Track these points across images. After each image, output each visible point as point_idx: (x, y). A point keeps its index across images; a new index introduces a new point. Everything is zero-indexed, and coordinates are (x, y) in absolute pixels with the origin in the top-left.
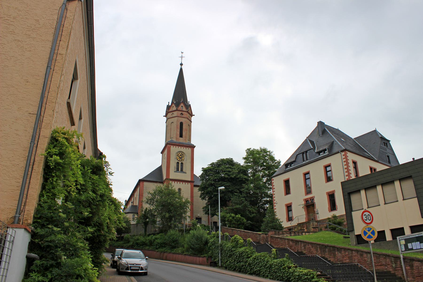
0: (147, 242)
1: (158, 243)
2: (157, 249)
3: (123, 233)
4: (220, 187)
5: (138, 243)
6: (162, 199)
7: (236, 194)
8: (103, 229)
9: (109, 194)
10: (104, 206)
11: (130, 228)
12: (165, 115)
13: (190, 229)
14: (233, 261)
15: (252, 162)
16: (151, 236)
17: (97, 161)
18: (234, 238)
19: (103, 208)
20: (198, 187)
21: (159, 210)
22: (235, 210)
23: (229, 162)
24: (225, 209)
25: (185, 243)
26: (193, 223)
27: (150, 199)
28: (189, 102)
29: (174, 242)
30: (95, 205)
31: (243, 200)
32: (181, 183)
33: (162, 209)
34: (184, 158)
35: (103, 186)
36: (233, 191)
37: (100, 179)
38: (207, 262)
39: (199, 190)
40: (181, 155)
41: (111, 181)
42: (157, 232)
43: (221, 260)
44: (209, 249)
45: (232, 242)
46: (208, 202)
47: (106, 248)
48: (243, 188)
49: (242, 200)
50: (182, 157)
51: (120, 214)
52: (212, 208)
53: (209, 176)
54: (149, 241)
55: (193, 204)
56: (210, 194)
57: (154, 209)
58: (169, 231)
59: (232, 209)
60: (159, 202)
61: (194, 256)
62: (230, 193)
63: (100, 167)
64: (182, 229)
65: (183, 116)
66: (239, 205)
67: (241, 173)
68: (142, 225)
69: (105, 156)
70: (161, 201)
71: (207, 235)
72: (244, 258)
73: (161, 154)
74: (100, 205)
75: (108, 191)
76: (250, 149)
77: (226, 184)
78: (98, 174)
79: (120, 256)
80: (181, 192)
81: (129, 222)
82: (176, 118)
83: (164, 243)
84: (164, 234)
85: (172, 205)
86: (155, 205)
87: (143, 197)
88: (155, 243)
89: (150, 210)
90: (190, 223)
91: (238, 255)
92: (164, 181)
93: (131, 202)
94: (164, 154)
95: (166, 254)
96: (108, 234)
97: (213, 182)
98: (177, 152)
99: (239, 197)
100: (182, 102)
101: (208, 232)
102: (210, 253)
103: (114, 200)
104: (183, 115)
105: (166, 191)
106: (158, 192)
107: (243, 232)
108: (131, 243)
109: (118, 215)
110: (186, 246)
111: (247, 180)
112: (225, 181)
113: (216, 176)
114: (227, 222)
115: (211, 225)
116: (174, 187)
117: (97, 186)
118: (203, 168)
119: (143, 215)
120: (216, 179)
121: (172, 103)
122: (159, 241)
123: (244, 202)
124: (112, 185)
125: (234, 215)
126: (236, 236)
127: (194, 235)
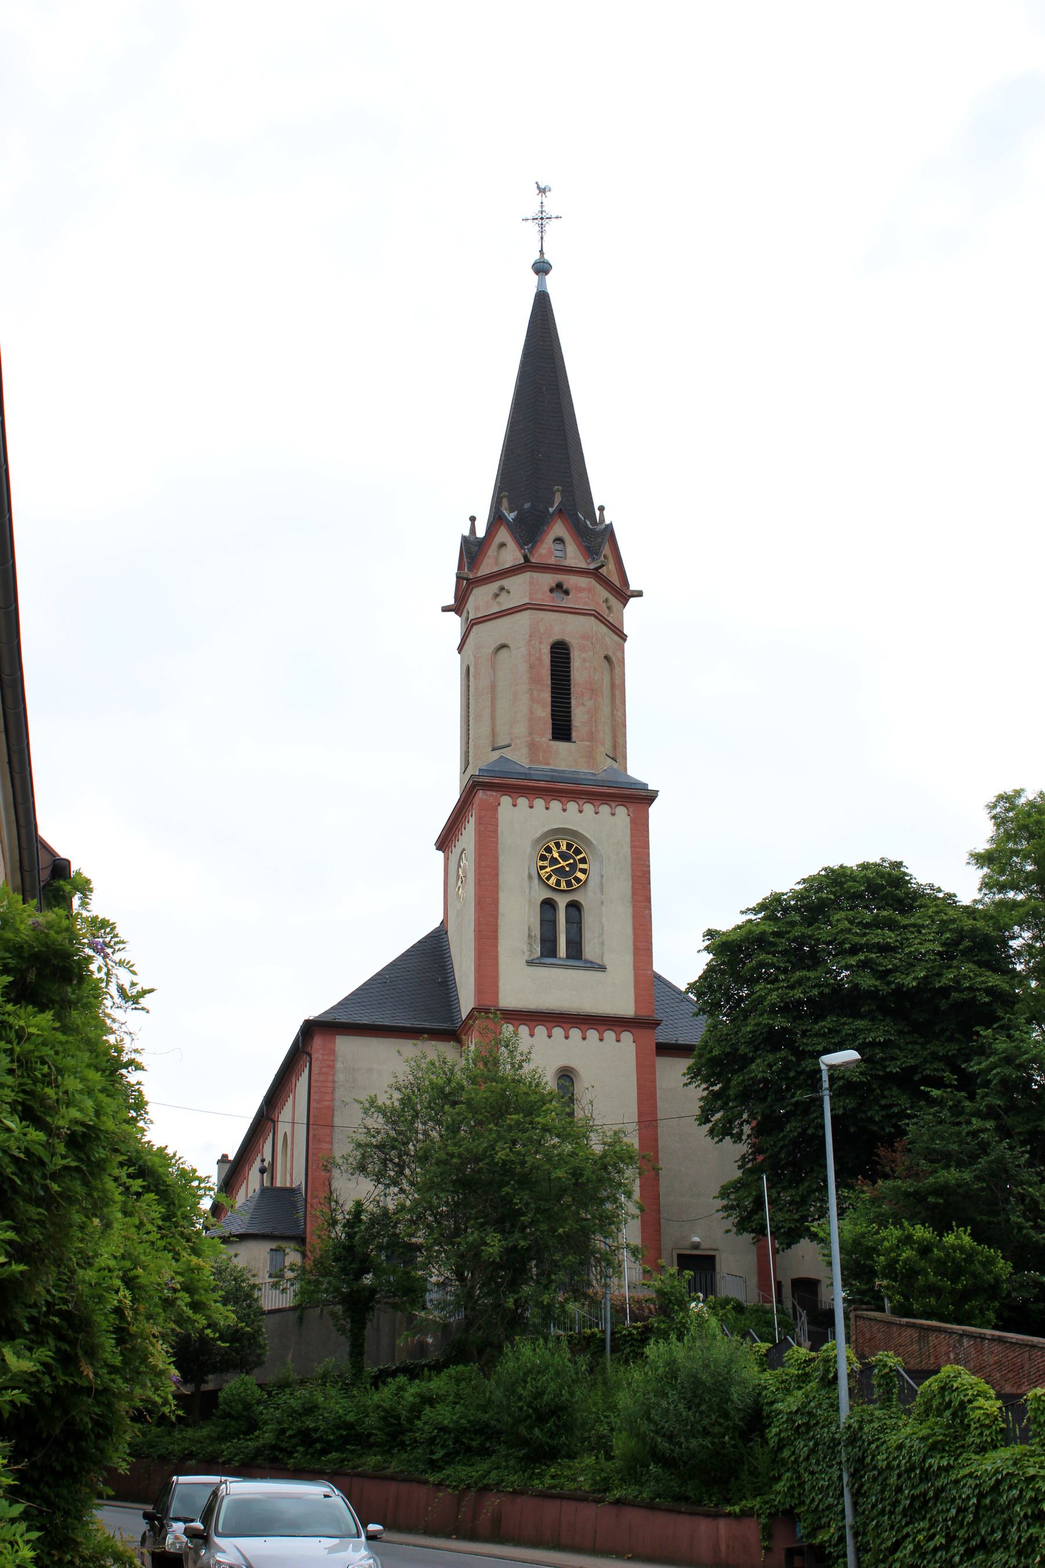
0: (372, 1421)
1: (443, 1429)
2: (434, 1466)
3: (215, 1370)
4: (827, 1051)
5: (315, 1436)
6: (455, 1144)
7: (935, 1093)
8: (92, 1353)
9: (125, 1126)
10: (98, 1206)
11: (258, 1331)
12: (451, 601)
13: (646, 1334)
14: (939, 1540)
15: (1029, 878)
16: (393, 1384)
17: (41, 918)
18: (935, 1387)
19: (89, 1215)
20: (687, 1056)
21: (441, 1214)
22: (931, 1199)
23: (883, 887)
24: (866, 1196)
25: (616, 1422)
26: (660, 1292)
27: (381, 1147)
28: (602, 509)
29: (541, 1419)
30: (38, 1202)
31: (984, 1136)
32: (575, 1033)
33: (457, 1204)
34: (583, 871)
35: (83, 1079)
36: (916, 1078)
37: (64, 1033)
38: (766, 1548)
39: (694, 1073)
40: (564, 856)
41: (137, 1045)
42: (433, 1357)
43: (856, 1535)
44: (775, 1460)
45: (927, 1413)
46: (757, 1150)
47: (112, 1471)
48: (982, 1051)
49: (974, 1134)
50: (573, 866)
51: (196, 1252)
52: (784, 1189)
53: (756, 981)
54: (385, 1419)
55: (656, 1170)
56: (764, 1099)
57: (410, 1211)
58: (507, 1349)
59: (916, 1193)
60: (438, 1163)
61: (679, 1512)
62: (895, 1091)
63: (66, 955)
64: (594, 1335)
65: (568, 602)
66: (960, 1165)
67: (964, 953)
68: (334, 1315)
69: (88, 882)
70: (452, 1156)
71: (756, 1368)
72: (1010, 1521)
73: (440, 854)
74: (71, 1200)
75: (114, 1108)
76: (1018, 793)
77: (870, 1030)
78: (53, 1002)
79: (198, 1525)
80: (578, 1089)
81: (248, 1296)
82: (526, 615)
83: (482, 1430)
84: (475, 1366)
85: (525, 1182)
86: (412, 1184)
87: (331, 1136)
88: (423, 1428)
89: (384, 1218)
90: (642, 1294)
91: (968, 1498)
92: (464, 1028)
93: (257, 1165)
94: (456, 852)
95: (492, 1502)
96: (126, 1380)
97: (780, 1023)
99: (957, 1110)
100: (560, 512)
101: (764, 1346)
102: (780, 1486)
103: (156, 1159)
105: (481, 1093)
106: (433, 1100)
107: (997, 1348)
108: (267, 1436)
109: (185, 1255)
110: (621, 1444)
111: (1008, 1000)
112: (857, 1015)
113: (800, 982)
114: (885, 1283)
115: (779, 1301)
116: (528, 1060)
117: (48, 1080)
118: (711, 934)
119: (335, 1247)
120: (800, 1002)
121: (496, 520)
122: (444, 1415)
123: (989, 1144)
124: (139, 1067)
125: (927, 1235)
126: (947, 1370)
127: (672, 1371)
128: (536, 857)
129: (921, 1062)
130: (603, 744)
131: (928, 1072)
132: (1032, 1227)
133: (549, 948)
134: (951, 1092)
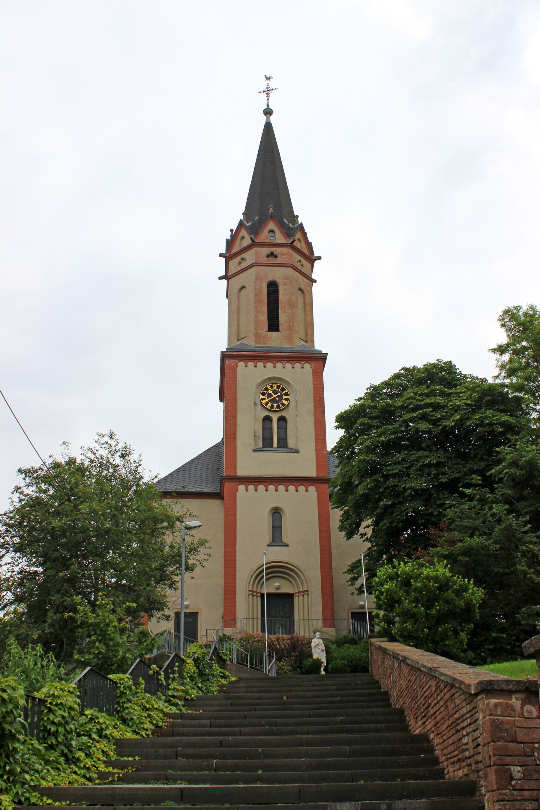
12: (223, 274)
34: (287, 400)
40: (275, 392)
50: (280, 397)
77: (428, 456)
82: (254, 269)
98: (259, 381)
104: (276, 257)
113: (384, 433)
128: (259, 393)
129: (463, 475)
130: (298, 333)
131: (467, 481)
132: (533, 573)
133: (267, 442)
134: (479, 489)
